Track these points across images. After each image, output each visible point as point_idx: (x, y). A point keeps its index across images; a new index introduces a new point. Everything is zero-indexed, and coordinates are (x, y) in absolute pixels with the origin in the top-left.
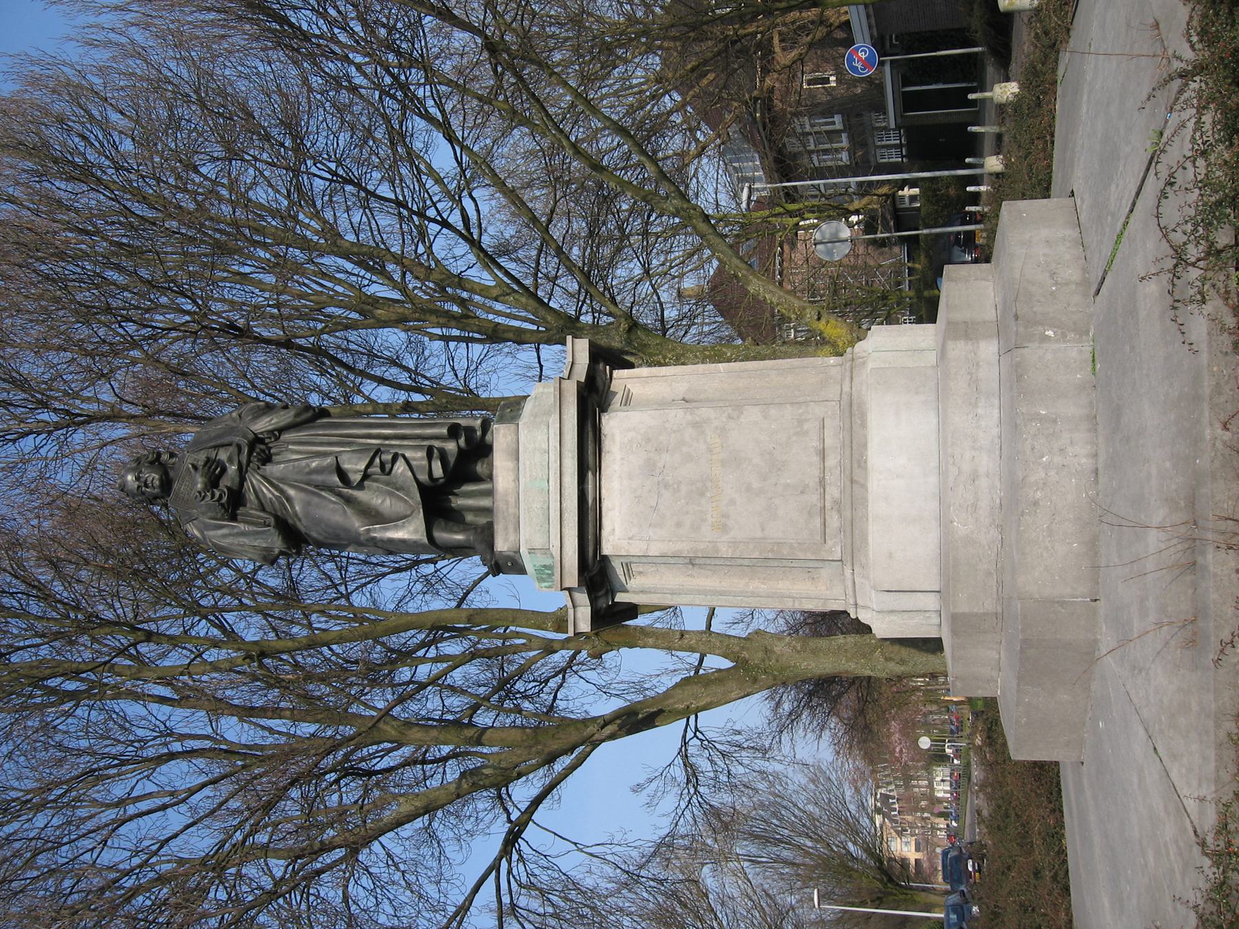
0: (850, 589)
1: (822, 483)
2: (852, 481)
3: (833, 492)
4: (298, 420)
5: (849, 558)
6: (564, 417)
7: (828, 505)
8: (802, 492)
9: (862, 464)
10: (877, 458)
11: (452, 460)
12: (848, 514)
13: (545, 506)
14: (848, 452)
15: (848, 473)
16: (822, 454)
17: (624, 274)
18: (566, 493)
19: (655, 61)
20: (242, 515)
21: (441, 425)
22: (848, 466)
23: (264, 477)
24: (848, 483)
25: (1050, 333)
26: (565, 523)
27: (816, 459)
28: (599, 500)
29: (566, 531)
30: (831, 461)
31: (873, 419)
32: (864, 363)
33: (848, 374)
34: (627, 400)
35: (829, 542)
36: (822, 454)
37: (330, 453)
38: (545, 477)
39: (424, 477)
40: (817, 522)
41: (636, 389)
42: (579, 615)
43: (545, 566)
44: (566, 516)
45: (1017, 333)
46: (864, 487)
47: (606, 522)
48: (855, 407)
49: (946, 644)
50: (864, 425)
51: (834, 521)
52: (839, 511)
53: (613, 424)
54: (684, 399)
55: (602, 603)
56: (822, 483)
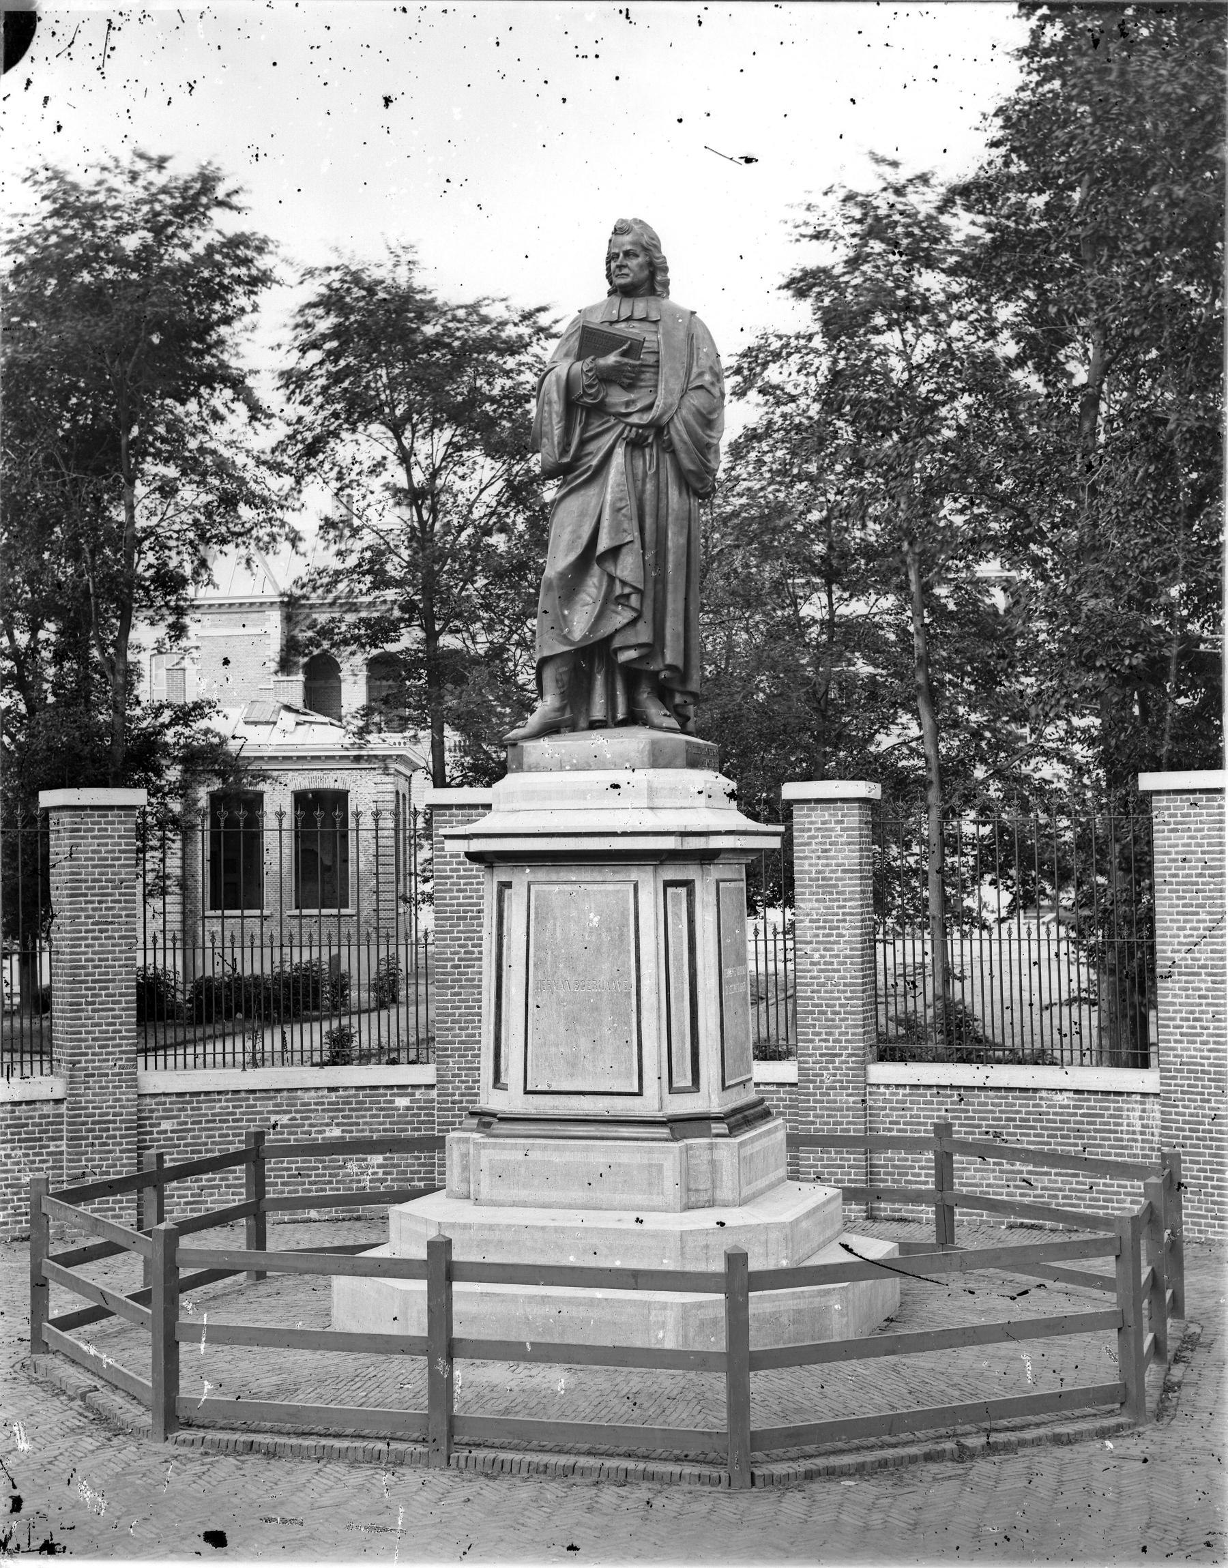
39: (616, 643)
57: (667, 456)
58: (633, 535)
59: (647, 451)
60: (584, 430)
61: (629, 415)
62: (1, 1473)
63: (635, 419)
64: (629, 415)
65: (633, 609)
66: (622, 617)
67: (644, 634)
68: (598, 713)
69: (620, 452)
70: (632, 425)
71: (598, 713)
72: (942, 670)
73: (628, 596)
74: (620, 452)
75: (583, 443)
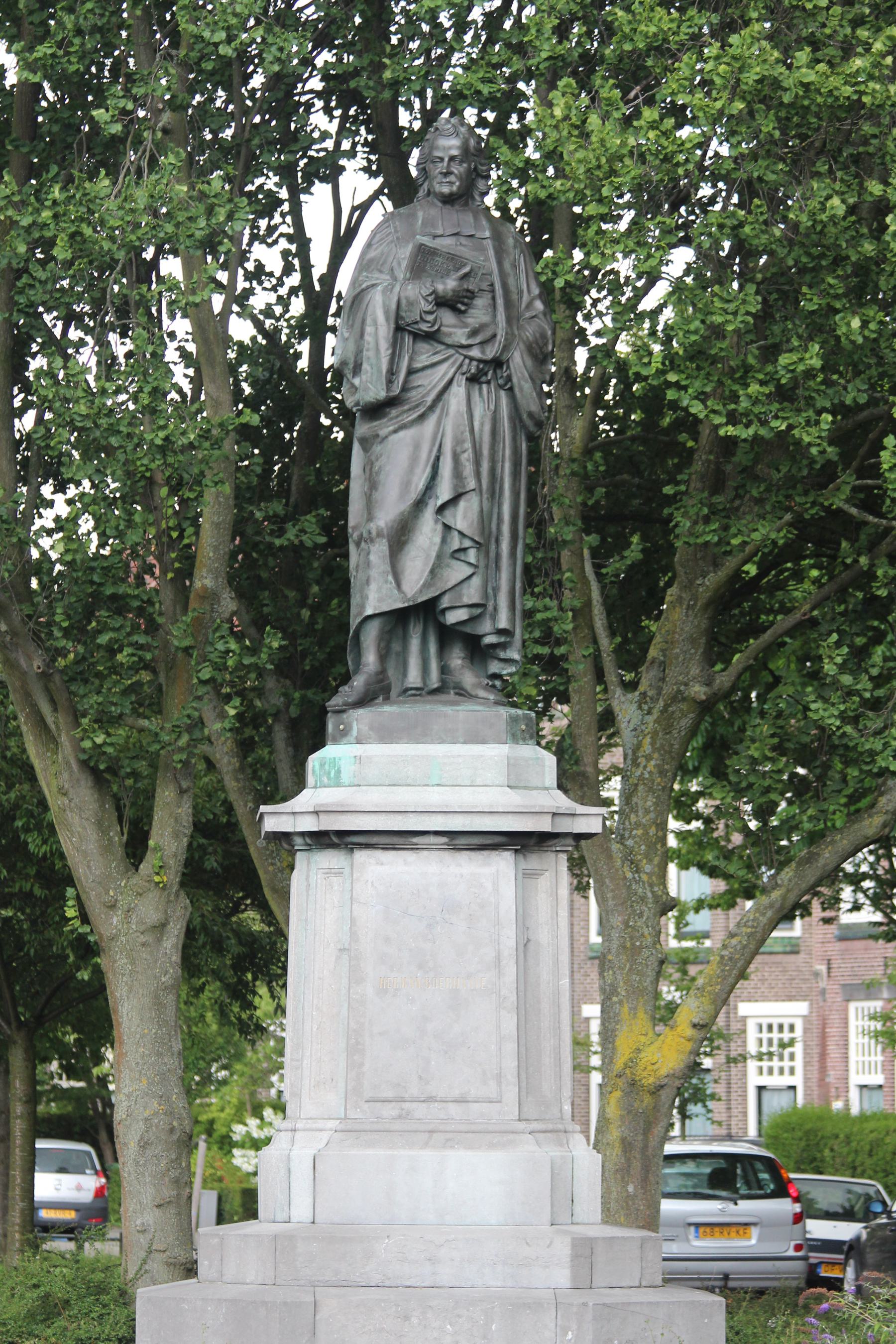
0: (314, 1126)
1: (430, 1099)
2: (431, 1132)
3: (420, 1110)
4: (525, 416)
5: (349, 1127)
6: (510, 817)
7: (407, 1105)
8: (420, 1078)
9: (448, 1144)
10: (459, 1160)
11: (468, 629)
12: (397, 1126)
13: (409, 781)
14: (463, 1128)
15: (441, 1128)
16: (461, 1100)
17: (443, 142)
18: (425, 817)
19: (844, 544)
20: (403, 339)
21: (512, 620)
22: (448, 1128)
23: (450, 382)
24: (430, 1127)
25: (570, 1336)
26: (392, 816)
27: (456, 1093)
28: (415, 848)
29: (383, 817)
30: (454, 1110)
31: (497, 1156)
32: (561, 1145)
33: (550, 1126)
34: (529, 875)
35: (367, 1105)
36: (461, 1100)
37: (696, 1138)
38: (443, 781)
39: (445, 602)
40: (389, 1094)
41: (544, 882)
42: (284, 818)
43: (339, 772)
44: (399, 817)
45: (571, 1305)
46: (426, 1145)
47: (391, 855)
48: (511, 1137)
49: (249, 1227)
50: (491, 1146)
51: (389, 1111)
52: (400, 1117)
53: (502, 865)
54: (528, 940)
55: (298, 840)
56: (430, 1099)
57: (503, 394)
58: (472, 484)
59: (485, 387)
60: (411, 359)
61: (469, 347)
62: (895, 1215)
63: (475, 353)
64: (469, 347)
65: (470, 564)
66: (457, 572)
67: (472, 593)
68: (414, 677)
69: (459, 391)
70: (472, 359)
71: (414, 677)
72: (55, 282)
73: (464, 550)
74: (459, 391)
75: (411, 372)
